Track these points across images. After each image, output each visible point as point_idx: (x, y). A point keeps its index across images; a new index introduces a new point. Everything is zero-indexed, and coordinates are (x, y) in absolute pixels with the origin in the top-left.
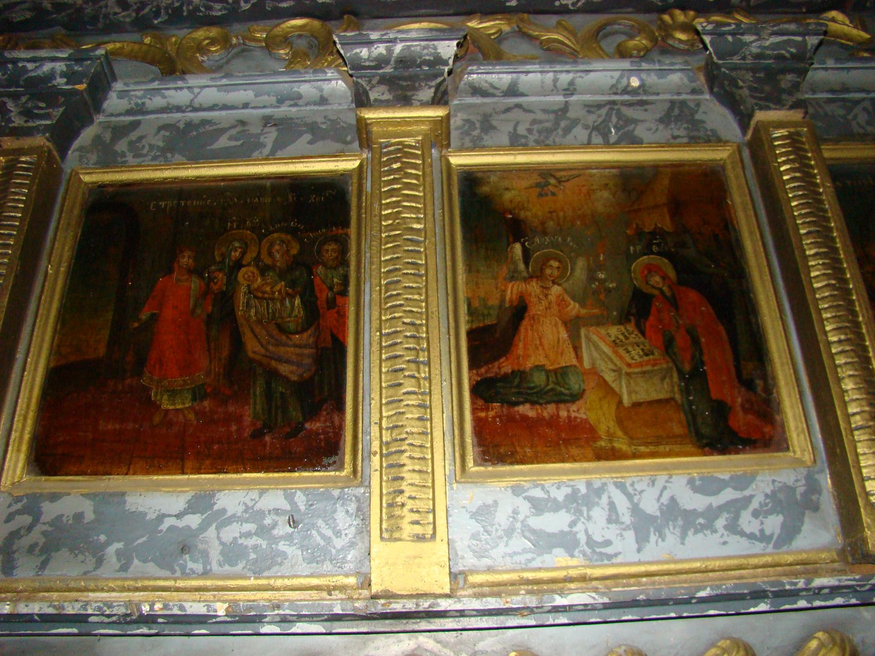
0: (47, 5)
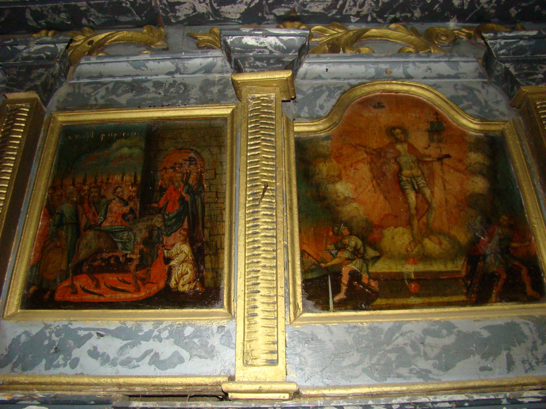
0: (83, 5)
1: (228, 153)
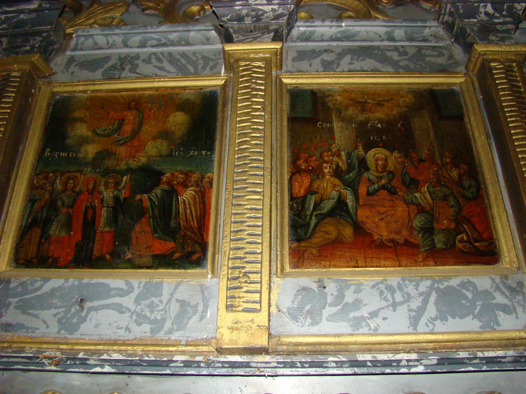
1: (467, 117)
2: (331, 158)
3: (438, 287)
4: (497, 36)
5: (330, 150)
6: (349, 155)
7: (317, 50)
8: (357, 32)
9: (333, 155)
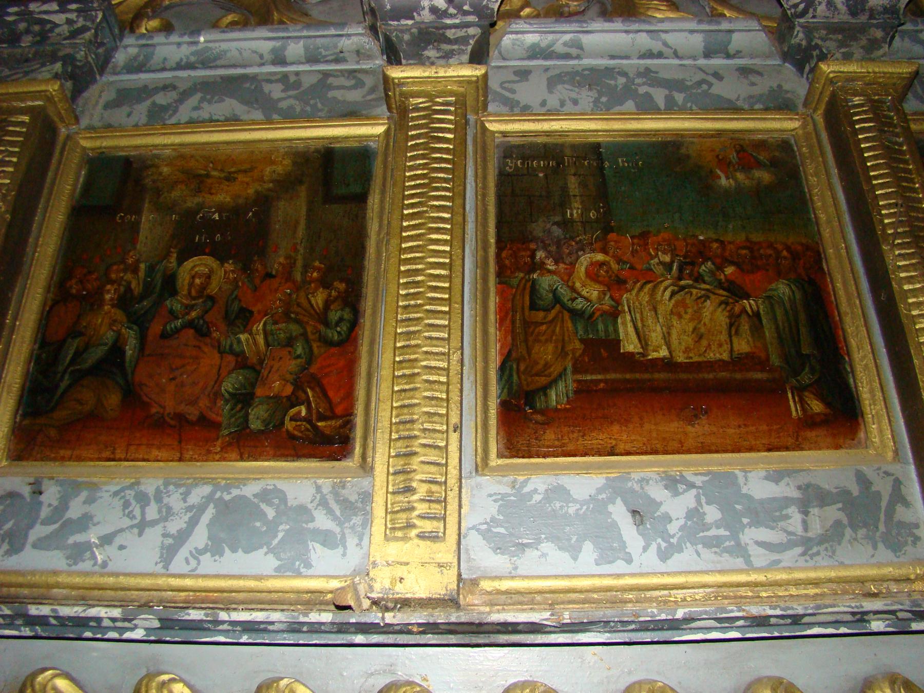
2: (122, 275)
3: (221, 498)
4: (438, 50)
5: (123, 261)
6: (151, 269)
7: (151, 87)
8: (223, 51)
9: (125, 271)
